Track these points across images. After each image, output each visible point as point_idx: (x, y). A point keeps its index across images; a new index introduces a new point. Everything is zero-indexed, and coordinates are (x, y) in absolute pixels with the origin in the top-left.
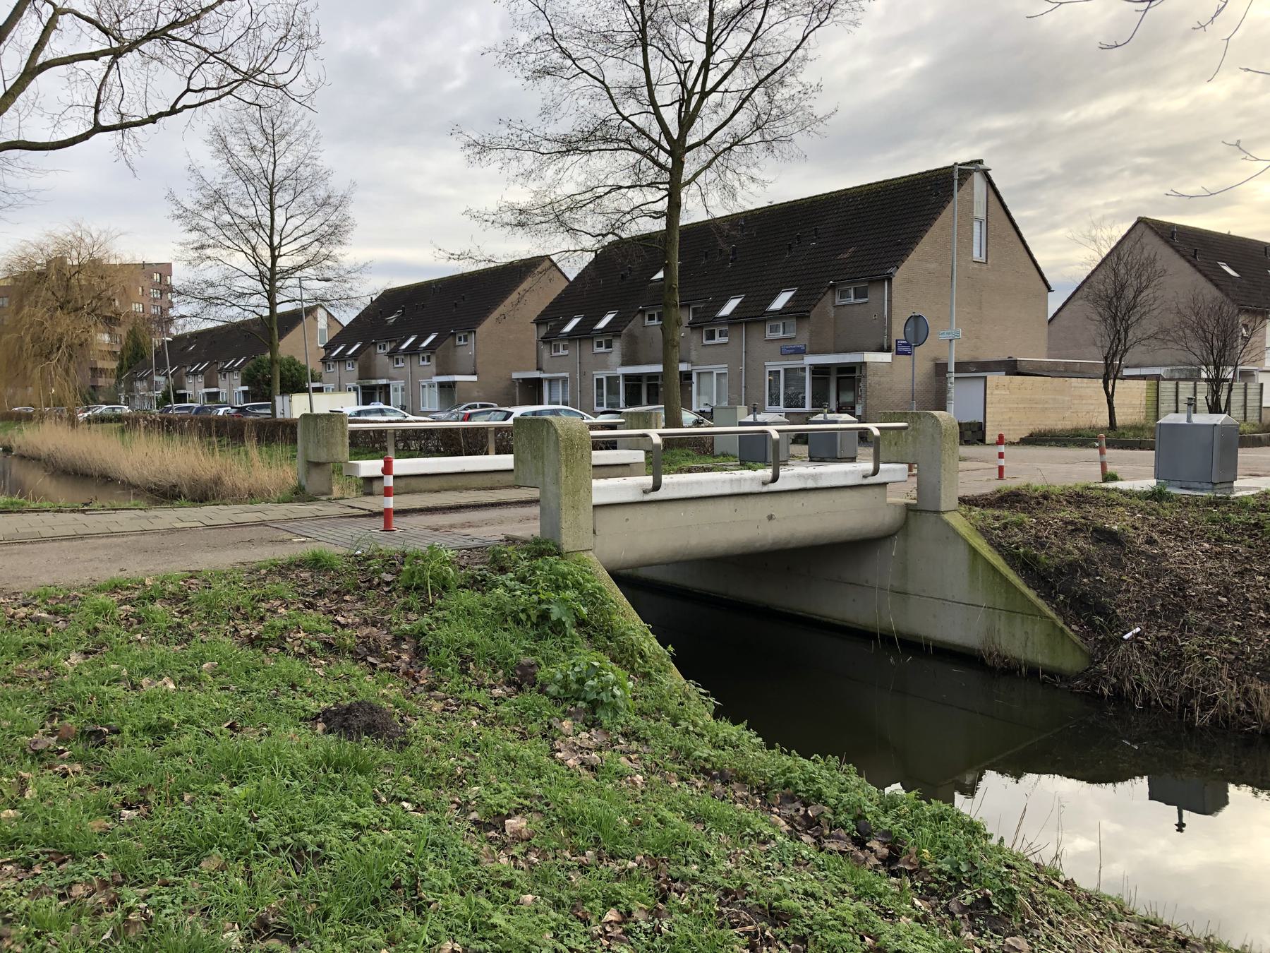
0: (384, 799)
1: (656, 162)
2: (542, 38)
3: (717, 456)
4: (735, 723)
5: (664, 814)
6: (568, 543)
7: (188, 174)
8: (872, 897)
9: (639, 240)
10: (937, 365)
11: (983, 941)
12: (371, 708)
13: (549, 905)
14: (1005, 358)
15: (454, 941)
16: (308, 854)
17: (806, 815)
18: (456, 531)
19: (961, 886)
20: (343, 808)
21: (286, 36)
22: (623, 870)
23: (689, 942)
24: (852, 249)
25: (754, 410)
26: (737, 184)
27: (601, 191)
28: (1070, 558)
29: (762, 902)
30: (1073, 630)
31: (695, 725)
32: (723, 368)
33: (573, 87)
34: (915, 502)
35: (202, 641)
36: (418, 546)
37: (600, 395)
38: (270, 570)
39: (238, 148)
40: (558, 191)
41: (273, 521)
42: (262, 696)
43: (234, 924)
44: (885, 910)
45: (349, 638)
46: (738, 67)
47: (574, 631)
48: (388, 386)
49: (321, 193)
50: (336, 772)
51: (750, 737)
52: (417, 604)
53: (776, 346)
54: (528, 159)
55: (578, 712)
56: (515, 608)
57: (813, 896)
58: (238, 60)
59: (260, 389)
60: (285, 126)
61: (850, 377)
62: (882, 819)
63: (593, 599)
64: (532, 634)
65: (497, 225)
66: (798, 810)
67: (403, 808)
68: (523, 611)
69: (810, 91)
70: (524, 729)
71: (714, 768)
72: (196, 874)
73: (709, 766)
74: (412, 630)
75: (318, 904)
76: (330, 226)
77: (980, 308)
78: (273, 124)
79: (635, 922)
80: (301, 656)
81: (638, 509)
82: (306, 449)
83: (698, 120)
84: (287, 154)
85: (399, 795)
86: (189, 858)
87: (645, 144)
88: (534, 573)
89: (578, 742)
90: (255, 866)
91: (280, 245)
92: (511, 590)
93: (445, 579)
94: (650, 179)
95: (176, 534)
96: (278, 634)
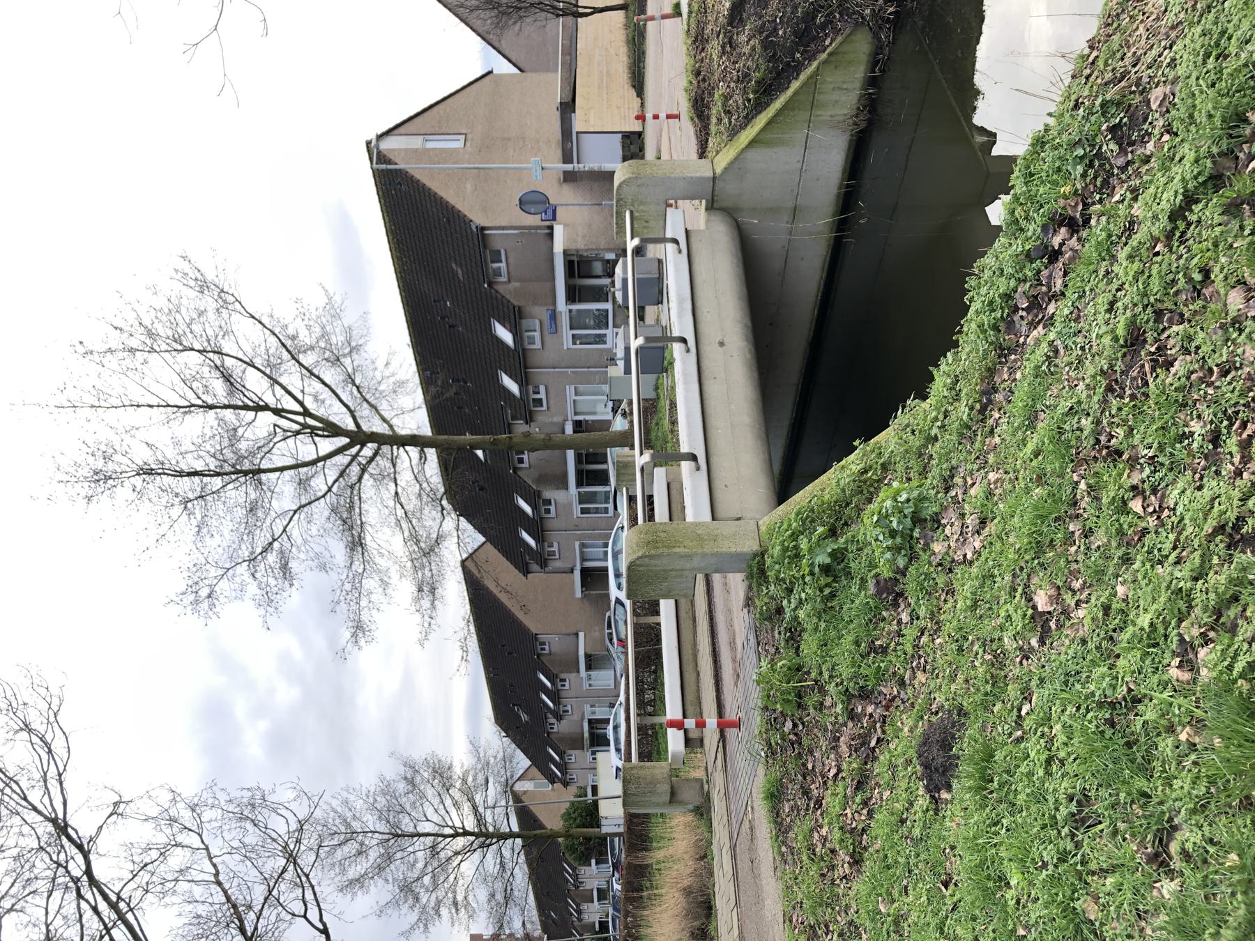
0: (1019, 733)
1: (372, 459)
2: (253, 570)
3: (658, 395)
4: (932, 379)
5: (1029, 452)
6: (751, 546)
7: (384, 917)
8: (1112, 243)
9: (447, 475)
10: (565, 180)
11: (1156, 132)
12: (925, 744)
13: (1127, 569)
14: (558, 114)
15: (1169, 665)
16: (1080, 812)
17: (1027, 310)
18: (739, 656)
19: (1099, 155)
20: (1030, 774)
21: (253, 821)
22: (1089, 493)
23: (1163, 428)
24: (454, 266)
25: (612, 360)
26: (392, 380)
27: (400, 512)
28: (758, 48)
29: (1119, 355)
30: (831, 44)
31: (936, 419)
32: (570, 390)
33: (300, 541)
34: (704, 201)
35: (857, 912)
36: (756, 696)
37: (597, 511)
38: (783, 842)
39: (359, 867)
40: (400, 553)
41: (731, 837)
42: (913, 853)
43: (1154, 887)
44: (1125, 230)
45: (851, 764)
46: (279, 380)
47: (842, 540)
48: (590, 721)
49: (402, 787)
50: (992, 781)
51: (947, 364)
52: (816, 697)
53: (548, 338)
54: (370, 583)
55: (925, 537)
56: (819, 599)
57: (1112, 304)
58: (276, 867)
59: (594, 848)
60: (338, 821)
61: (577, 266)
62: (1030, 234)
63: (808, 520)
64: (845, 582)
65: (434, 614)
66: (1022, 317)
67: (1028, 713)
68: (821, 590)
69: (302, 310)
70: (943, 590)
71: (980, 401)
72: (1102, 924)
73: (978, 406)
74: (843, 702)
75: (1133, 802)
76: (434, 778)
77: (509, 139)
78: (336, 833)
79: (1144, 482)
80: (870, 814)
81: (714, 474)
82: (658, 805)
83: (331, 419)
84: (365, 820)
85: (1014, 718)
86: (1085, 931)
87: (355, 469)
88: (783, 580)
89: (956, 537)
90: (1093, 866)
91: (453, 827)
92: (801, 601)
93: (789, 669)
94: (389, 465)
95: (746, 935)
96: (848, 836)
